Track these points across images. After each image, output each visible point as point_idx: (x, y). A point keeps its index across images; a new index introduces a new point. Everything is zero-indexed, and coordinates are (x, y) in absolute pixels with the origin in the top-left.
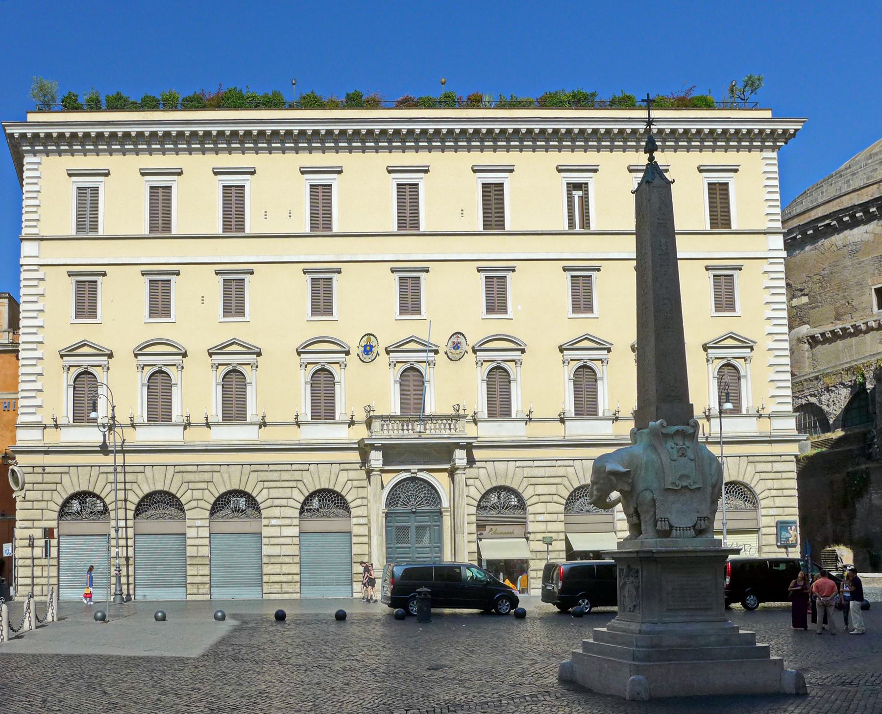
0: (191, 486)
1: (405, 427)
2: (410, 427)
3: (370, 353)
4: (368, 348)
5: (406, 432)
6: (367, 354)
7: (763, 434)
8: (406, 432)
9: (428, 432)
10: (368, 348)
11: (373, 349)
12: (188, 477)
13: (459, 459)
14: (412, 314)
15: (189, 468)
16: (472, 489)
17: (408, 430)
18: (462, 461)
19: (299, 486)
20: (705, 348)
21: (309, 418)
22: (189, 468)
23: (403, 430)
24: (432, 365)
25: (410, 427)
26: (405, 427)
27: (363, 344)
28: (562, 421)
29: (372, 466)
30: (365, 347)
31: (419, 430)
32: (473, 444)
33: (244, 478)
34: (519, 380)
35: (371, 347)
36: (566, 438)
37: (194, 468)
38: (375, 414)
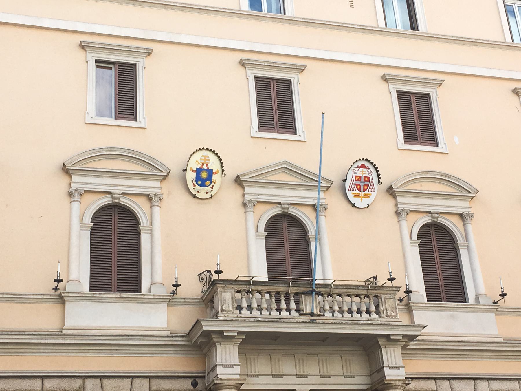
1: (283, 305)
2: (293, 305)
3: (207, 183)
4: (204, 175)
5: (285, 314)
6: (203, 185)
8: (245, 312)
9: (328, 315)
10: (204, 175)
11: (214, 177)
13: (391, 368)
14: (279, 132)
17: (288, 310)
18: (229, 370)
20: (66, 170)
21: (86, 287)
23: (279, 310)
24: (156, 202)
25: (293, 305)
26: (283, 305)
27: (195, 167)
28: (61, 300)
29: (220, 377)
30: (199, 171)
31: (309, 311)
32: (392, 337)
34: (473, 243)
35: (210, 173)
36: (64, 332)
38: (222, 277)
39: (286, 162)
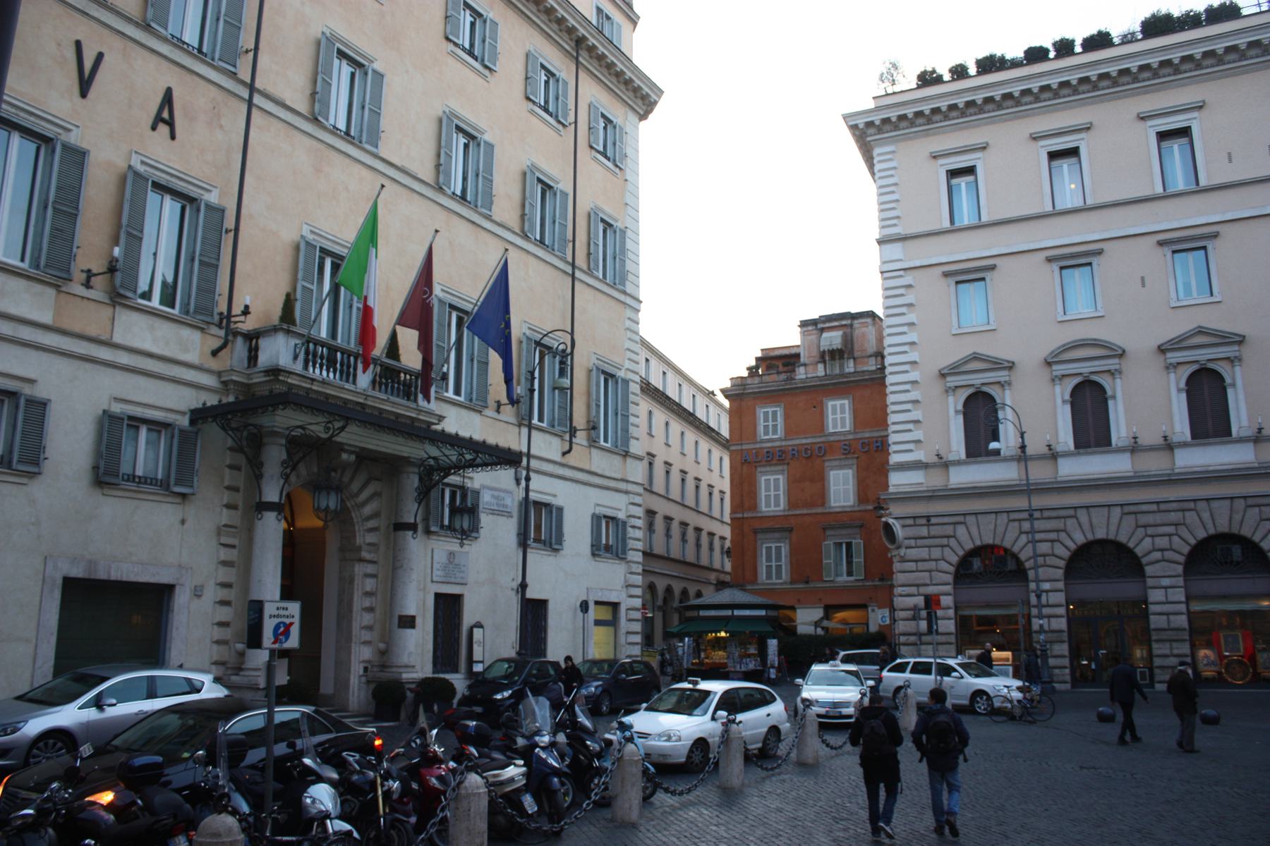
0: (1150, 531)
7: (1138, 474)
12: (1144, 519)
15: (1144, 508)
16: (1176, 539)
19: (1180, 533)
22: (1144, 508)
33: (1238, 517)
34: (1239, 382)
37: (1154, 507)
39: (974, 353)
